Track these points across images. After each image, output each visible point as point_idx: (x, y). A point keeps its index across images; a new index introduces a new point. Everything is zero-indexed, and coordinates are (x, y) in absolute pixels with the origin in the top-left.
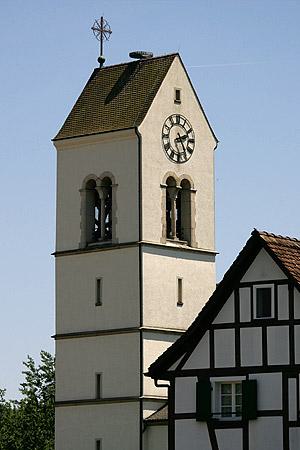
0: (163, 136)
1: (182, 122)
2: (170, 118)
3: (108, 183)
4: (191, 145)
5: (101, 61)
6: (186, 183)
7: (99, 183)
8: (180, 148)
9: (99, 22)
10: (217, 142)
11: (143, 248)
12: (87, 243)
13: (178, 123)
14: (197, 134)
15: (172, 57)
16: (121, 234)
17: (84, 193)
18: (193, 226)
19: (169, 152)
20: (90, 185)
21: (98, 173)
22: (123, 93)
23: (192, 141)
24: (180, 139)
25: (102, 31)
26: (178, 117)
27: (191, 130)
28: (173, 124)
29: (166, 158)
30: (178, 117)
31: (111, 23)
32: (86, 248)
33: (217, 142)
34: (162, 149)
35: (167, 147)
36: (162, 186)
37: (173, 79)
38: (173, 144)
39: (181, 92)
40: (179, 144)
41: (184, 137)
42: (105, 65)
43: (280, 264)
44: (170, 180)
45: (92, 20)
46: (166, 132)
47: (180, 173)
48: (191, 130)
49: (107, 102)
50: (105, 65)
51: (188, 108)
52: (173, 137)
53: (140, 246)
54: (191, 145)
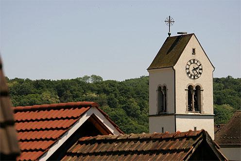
0: (186, 69)
1: (196, 62)
2: (190, 61)
3: (165, 87)
4: (200, 71)
5: (169, 34)
6: (198, 88)
7: (162, 88)
8: (196, 72)
9: (168, 18)
10: (214, 68)
11: (176, 116)
12: (159, 112)
13: (194, 62)
14: (204, 66)
15: (191, 35)
16: (170, 110)
17: (158, 92)
18: (202, 104)
19: (190, 75)
20: (160, 88)
21: (162, 84)
22: (173, 50)
23: (201, 69)
24: (195, 69)
25: (170, 22)
26: (194, 60)
27: (200, 65)
28: (191, 63)
29: (188, 78)
30: (194, 60)
31: (173, 18)
32: (159, 115)
33: (214, 68)
34: (186, 74)
35: (188, 73)
36: (186, 90)
37: (191, 44)
38: (191, 72)
39: (196, 50)
40: (195, 71)
41: (197, 68)
42: (171, 36)
43: (178, 151)
44: (190, 87)
45: (166, 18)
46: (188, 67)
47: (194, 83)
48: (200, 65)
49: (167, 54)
50: (171, 36)
51: (199, 56)
52: (191, 68)
53: (175, 115)
54: (200, 71)
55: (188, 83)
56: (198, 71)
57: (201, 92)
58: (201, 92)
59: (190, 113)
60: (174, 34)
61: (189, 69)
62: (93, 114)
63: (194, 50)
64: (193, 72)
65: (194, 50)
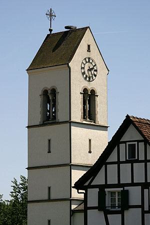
0: (82, 68)
1: (91, 61)
2: (85, 59)
3: (54, 92)
4: (95, 73)
5: (51, 30)
6: (93, 91)
7: (49, 92)
8: (90, 74)
9: (50, 11)
10: (109, 71)
11: (72, 124)
12: (44, 121)
15: (85, 29)
16: (61, 117)
17: (42, 96)
19: (85, 76)
20: (45, 93)
21: (49, 87)
23: (96, 71)
24: (90, 70)
25: (51, 15)
26: (89, 58)
27: (95, 65)
28: (86, 62)
29: (83, 79)
30: (89, 58)
31: (56, 11)
32: (43, 124)
33: (109, 71)
35: (84, 73)
36: (81, 93)
37: (87, 39)
38: (86, 72)
40: (90, 72)
41: (92, 69)
42: (52, 32)
44: (85, 90)
45: (46, 10)
48: (95, 65)
50: (52, 32)
51: (94, 54)
52: (86, 68)
53: (70, 123)
54: (95, 73)
55: (83, 86)
56: (93, 72)
57: (96, 97)
58: (96, 97)
59: (84, 122)
60: (58, 28)
61: (84, 68)
62: (128, 115)
63: (89, 46)
64: (88, 73)
65: (89, 46)
